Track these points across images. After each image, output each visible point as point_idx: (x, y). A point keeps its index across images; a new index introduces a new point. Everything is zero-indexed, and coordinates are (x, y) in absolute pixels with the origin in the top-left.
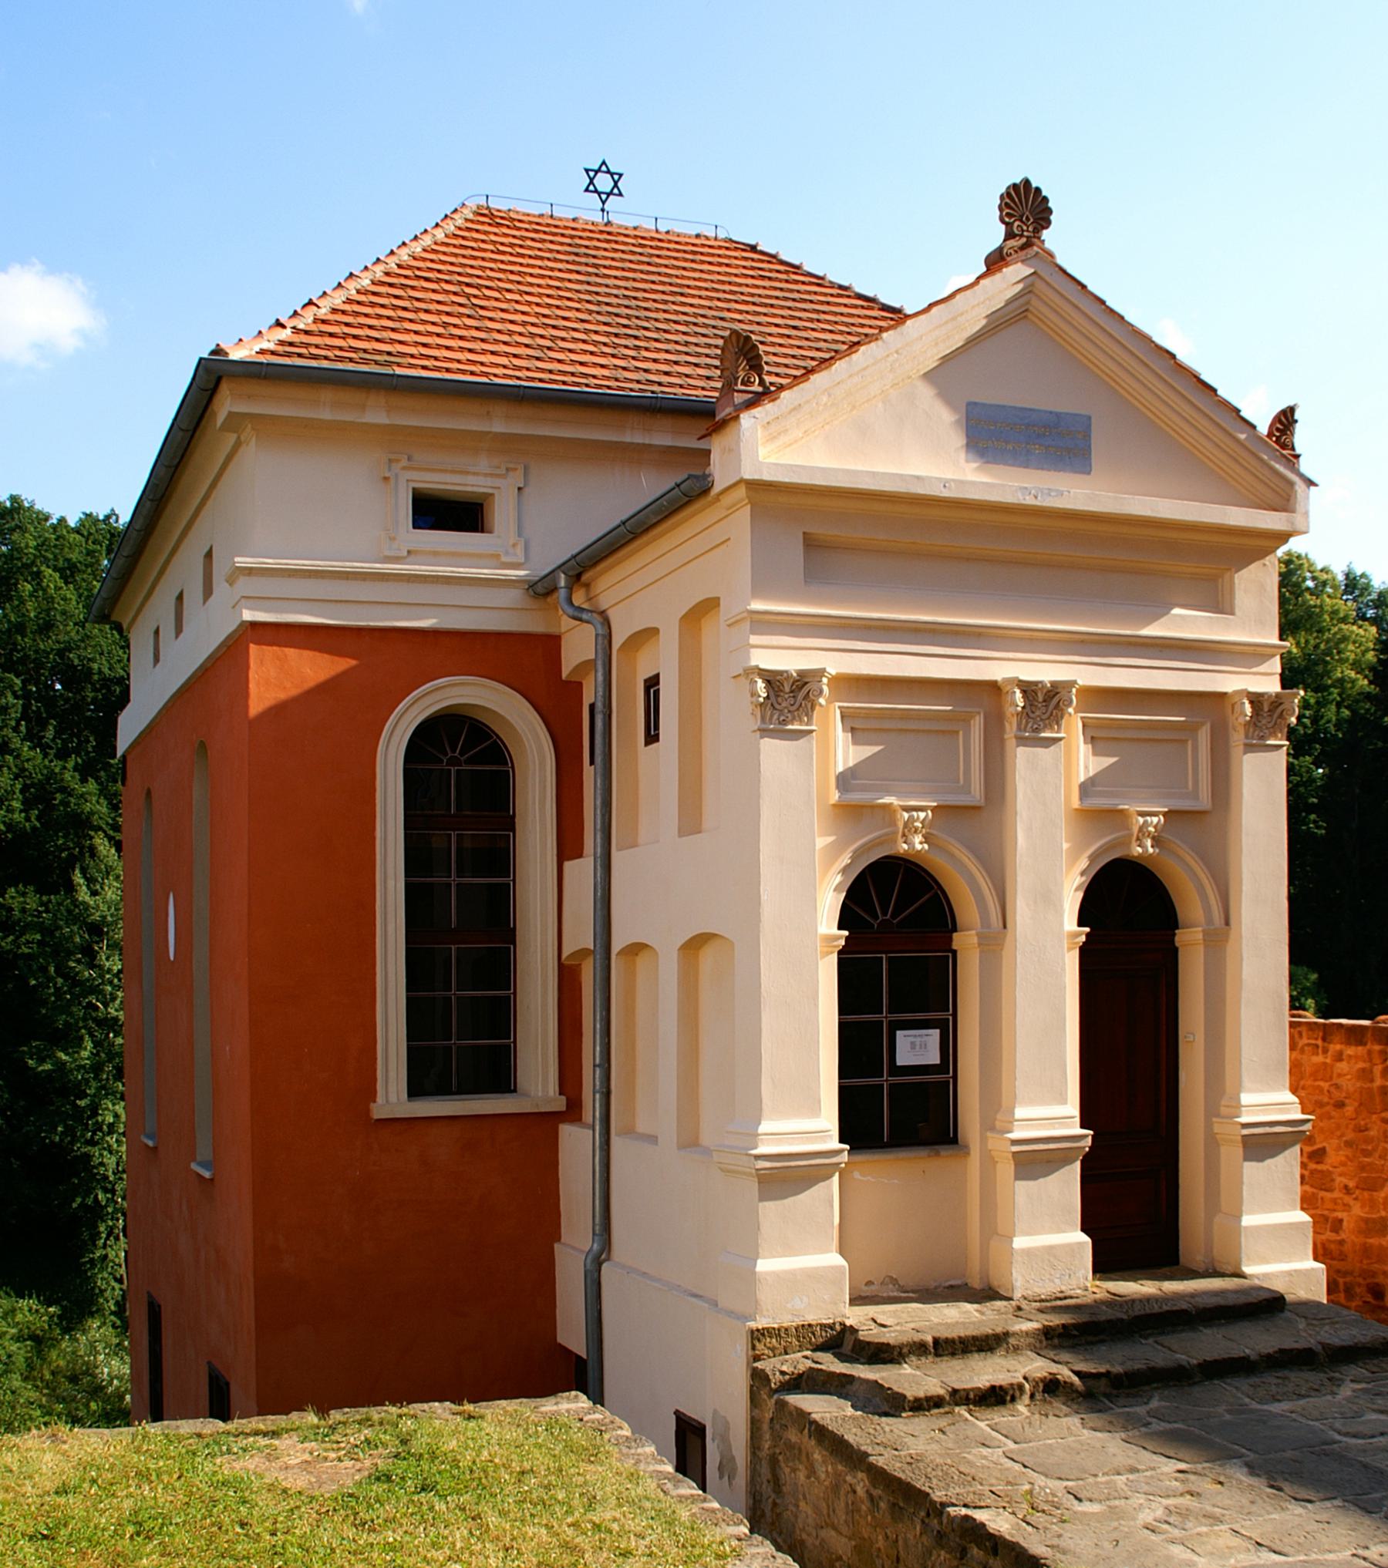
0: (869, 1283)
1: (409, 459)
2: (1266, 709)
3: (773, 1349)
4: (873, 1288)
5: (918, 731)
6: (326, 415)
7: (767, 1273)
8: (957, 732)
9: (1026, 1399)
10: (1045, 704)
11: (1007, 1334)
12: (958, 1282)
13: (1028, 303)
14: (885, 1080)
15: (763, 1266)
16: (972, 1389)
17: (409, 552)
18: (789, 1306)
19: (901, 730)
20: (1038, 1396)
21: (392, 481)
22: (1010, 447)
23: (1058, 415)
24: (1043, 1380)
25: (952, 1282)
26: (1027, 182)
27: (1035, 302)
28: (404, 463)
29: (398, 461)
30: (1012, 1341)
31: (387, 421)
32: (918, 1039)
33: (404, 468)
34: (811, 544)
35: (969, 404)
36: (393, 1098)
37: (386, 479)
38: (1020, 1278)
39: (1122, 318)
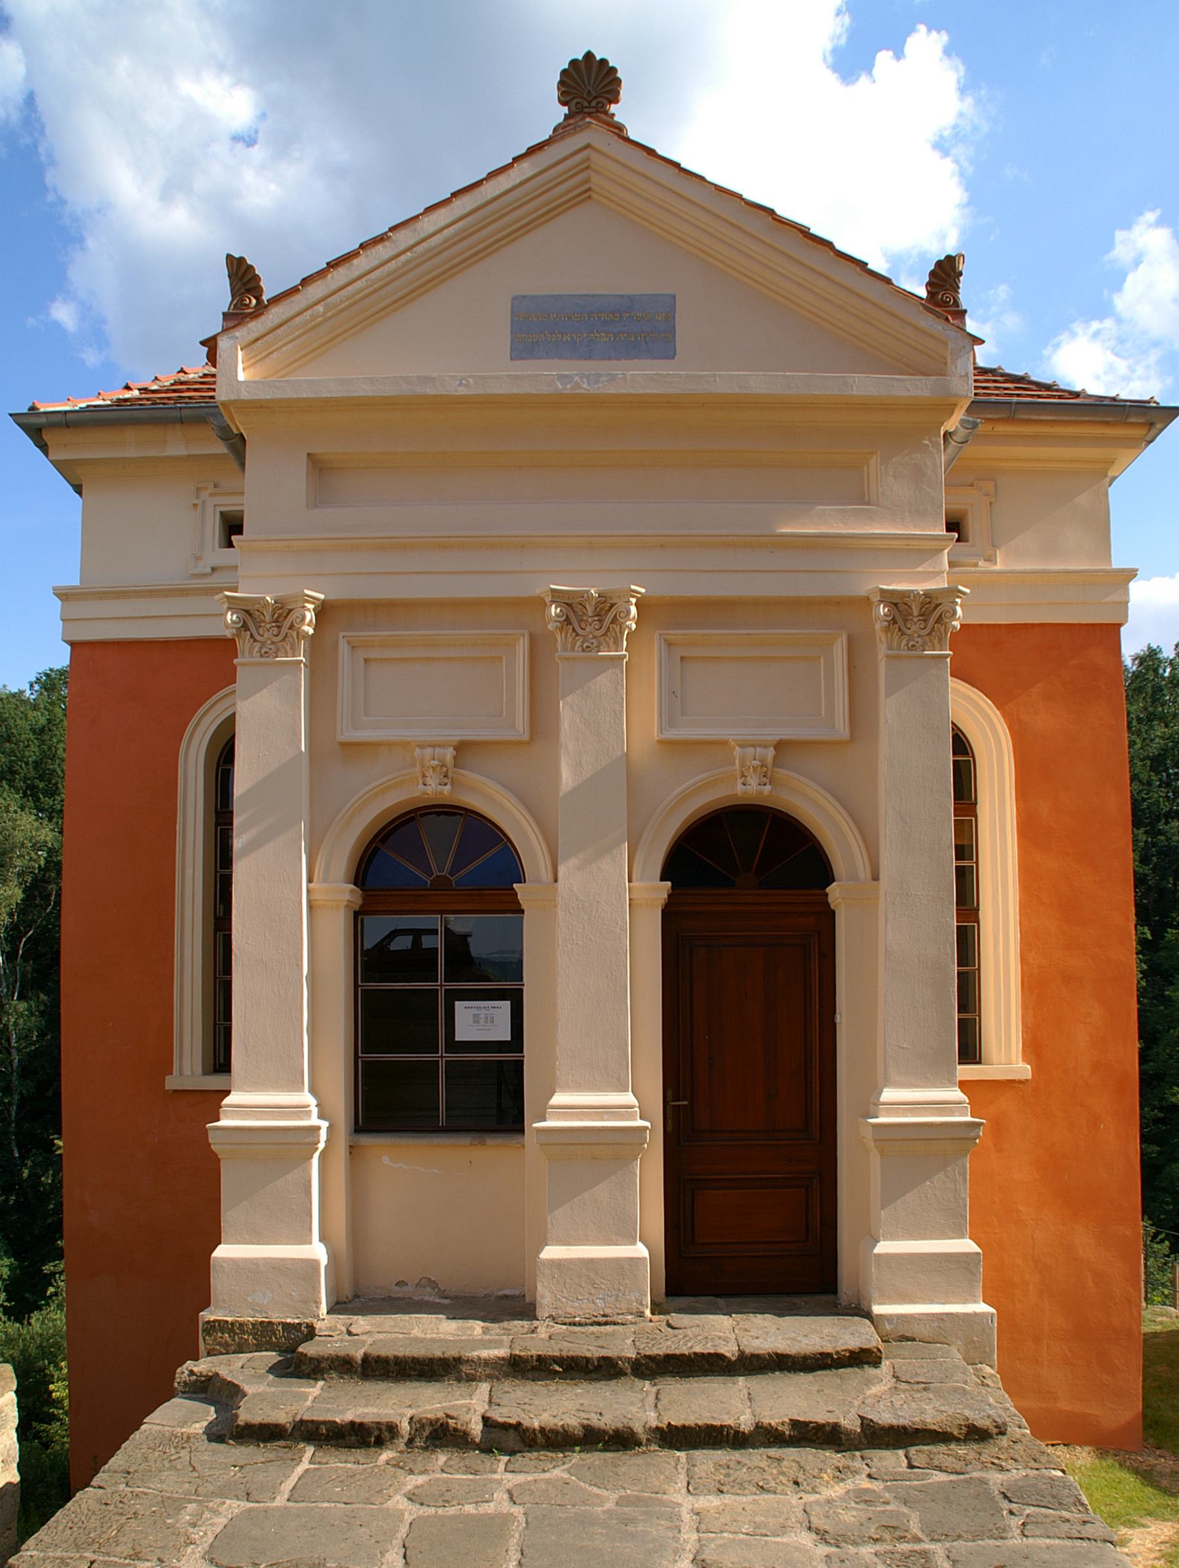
0: (401, 1283)
1: (216, 486)
2: (916, 613)
3: (227, 1345)
4: (405, 1288)
5: (450, 659)
6: (132, 453)
7: (224, 1260)
8: (500, 658)
9: (401, 1444)
10: (590, 618)
11: (458, 1360)
12: (517, 1292)
13: (588, 180)
14: (442, 1057)
15: (221, 1252)
16: (324, 1423)
17: (213, 569)
18: (249, 1299)
19: (427, 659)
20: (419, 1442)
21: (199, 508)
22: (567, 338)
23: (631, 298)
24: (431, 1423)
25: (508, 1292)
26: (589, 56)
27: (595, 178)
28: (211, 489)
29: (207, 488)
30: (465, 1369)
31: (186, 453)
32: (482, 1013)
33: (211, 495)
34: (318, 466)
35: (515, 298)
36: (187, 1071)
37: (195, 505)
38: (548, 1294)
39: (702, 178)
